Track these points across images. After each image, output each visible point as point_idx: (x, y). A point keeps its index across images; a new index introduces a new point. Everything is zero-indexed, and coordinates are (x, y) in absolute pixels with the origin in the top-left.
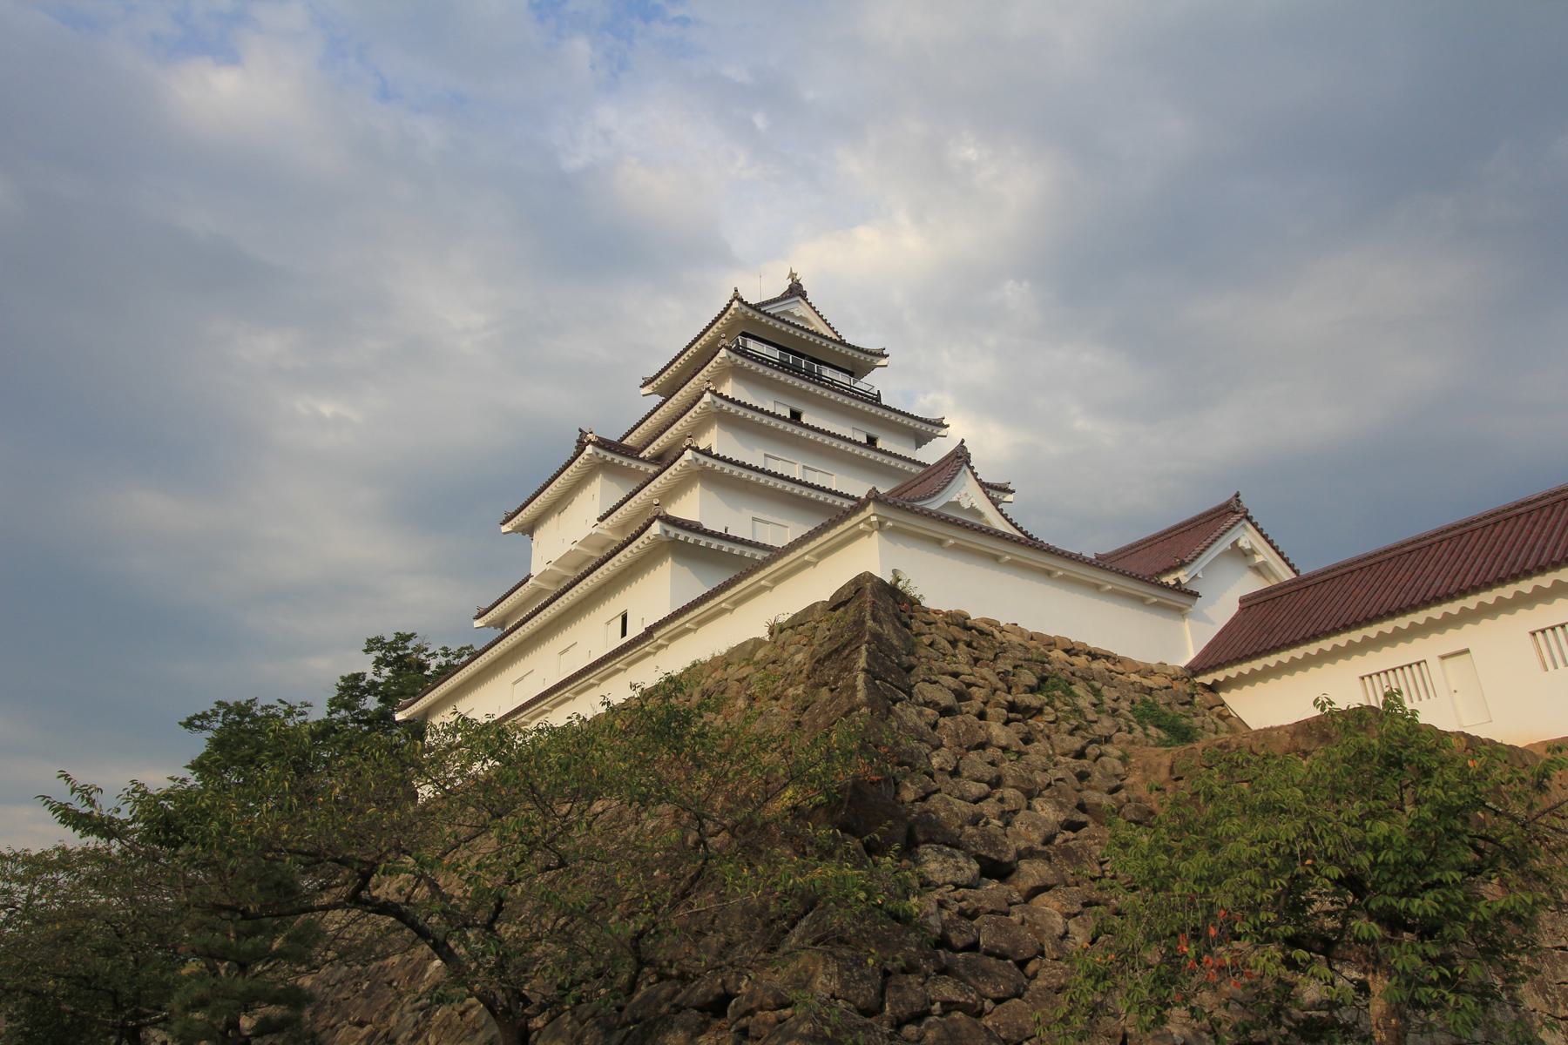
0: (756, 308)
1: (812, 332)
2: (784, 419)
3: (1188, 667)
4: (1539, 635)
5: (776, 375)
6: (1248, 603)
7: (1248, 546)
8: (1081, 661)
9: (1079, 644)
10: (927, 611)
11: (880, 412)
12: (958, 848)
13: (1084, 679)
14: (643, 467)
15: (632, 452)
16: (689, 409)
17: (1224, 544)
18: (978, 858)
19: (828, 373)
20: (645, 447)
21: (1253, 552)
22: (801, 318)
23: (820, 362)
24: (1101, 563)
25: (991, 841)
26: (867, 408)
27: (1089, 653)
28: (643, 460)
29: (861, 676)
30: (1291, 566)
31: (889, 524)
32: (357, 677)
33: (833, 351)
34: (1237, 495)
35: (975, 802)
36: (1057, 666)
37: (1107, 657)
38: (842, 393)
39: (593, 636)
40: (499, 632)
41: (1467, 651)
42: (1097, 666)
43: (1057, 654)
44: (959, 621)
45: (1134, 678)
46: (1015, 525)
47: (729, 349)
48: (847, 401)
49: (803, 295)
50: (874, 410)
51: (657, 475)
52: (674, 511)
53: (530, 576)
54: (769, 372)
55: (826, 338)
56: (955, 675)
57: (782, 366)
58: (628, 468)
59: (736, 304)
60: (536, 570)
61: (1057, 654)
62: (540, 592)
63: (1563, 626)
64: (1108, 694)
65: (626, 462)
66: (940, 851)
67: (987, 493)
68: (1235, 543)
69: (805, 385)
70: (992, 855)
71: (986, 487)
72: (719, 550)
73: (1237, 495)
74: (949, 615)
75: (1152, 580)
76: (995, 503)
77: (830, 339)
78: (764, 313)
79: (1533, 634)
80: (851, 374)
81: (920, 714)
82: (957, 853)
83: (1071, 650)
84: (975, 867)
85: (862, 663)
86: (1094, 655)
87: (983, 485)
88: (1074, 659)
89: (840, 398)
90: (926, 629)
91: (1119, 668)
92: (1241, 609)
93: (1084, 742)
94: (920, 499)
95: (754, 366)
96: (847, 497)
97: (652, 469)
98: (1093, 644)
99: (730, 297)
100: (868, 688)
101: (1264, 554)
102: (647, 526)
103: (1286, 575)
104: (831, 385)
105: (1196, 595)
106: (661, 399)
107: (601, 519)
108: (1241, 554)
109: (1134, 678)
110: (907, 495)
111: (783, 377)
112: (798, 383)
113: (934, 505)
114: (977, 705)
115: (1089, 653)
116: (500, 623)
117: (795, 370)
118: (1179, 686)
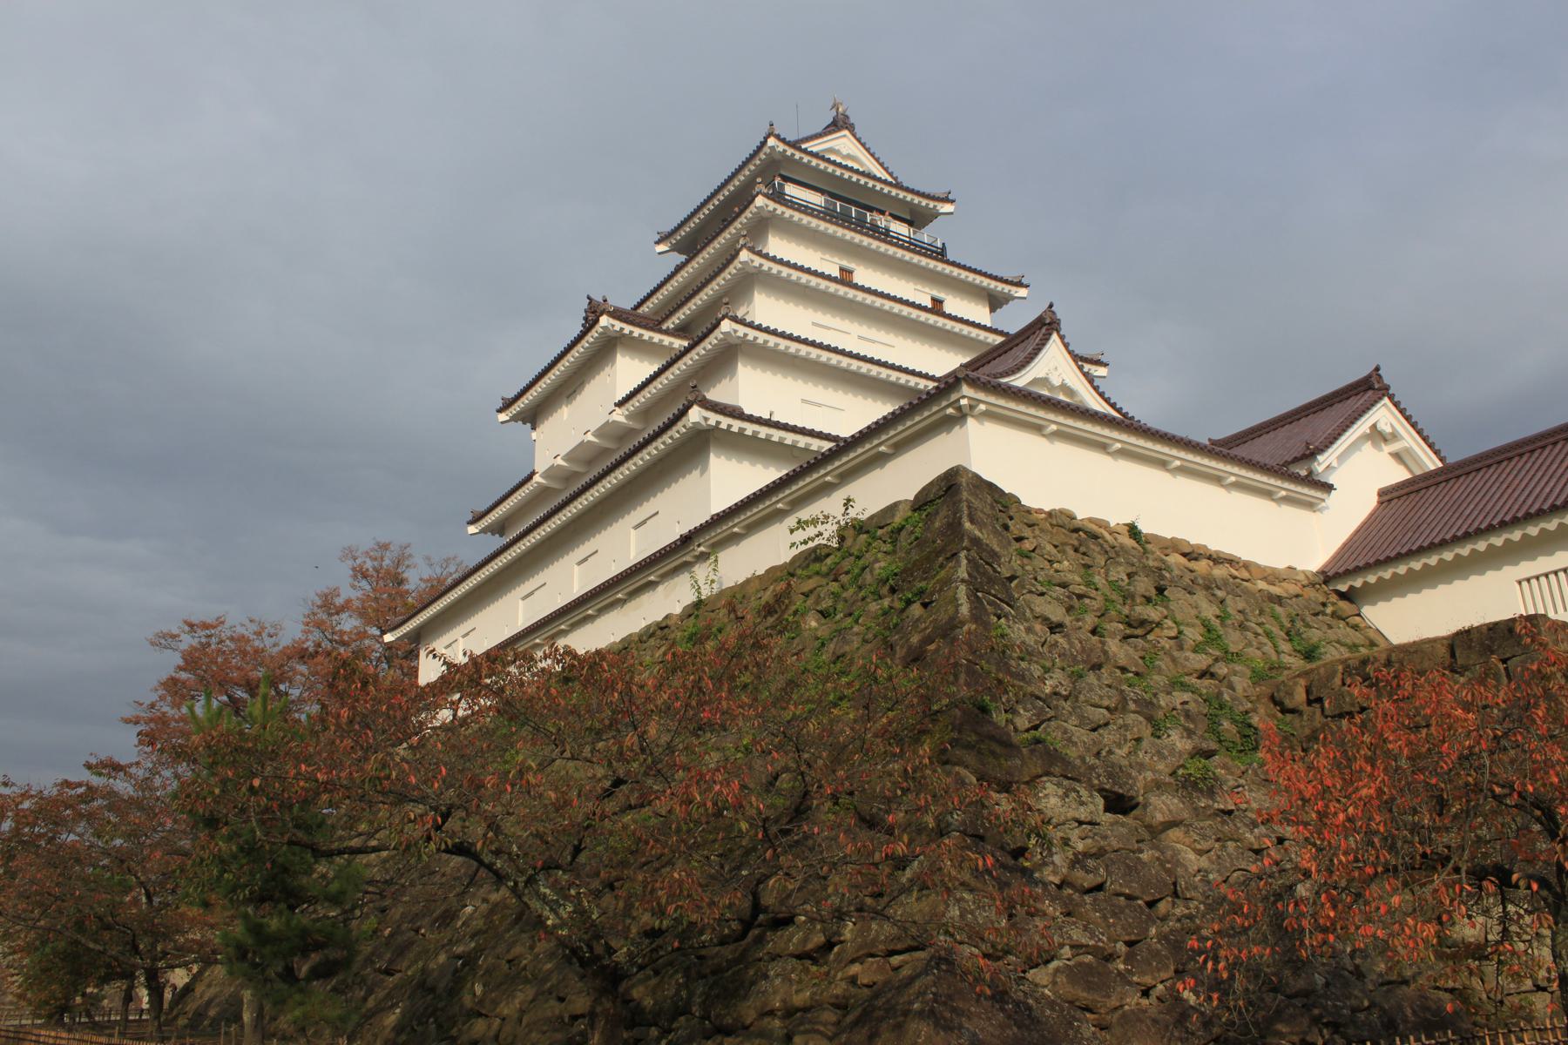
0: (795, 145)
1: (863, 174)
2: (925, 309)
3: (1322, 572)
4: (1525, 584)
5: (823, 226)
6: (1388, 496)
7: (1388, 430)
8: (1202, 566)
9: (1199, 546)
10: (1029, 511)
11: (948, 269)
12: (1079, 781)
13: (1207, 588)
14: (667, 340)
15: (654, 324)
16: (721, 270)
17: (1362, 427)
18: (1101, 791)
19: (882, 221)
20: (668, 317)
21: (1395, 436)
22: (849, 157)
23: (871, 209)
24: (1224, 449)
25: (1114, 772)
26: (932, 264)
27: (1210, 558)
28: (667, 332)
29: (963, 589)
30: (1436, 453)
31: (982, 407)
32: (335, 592)
33: (888, 195)
34: (1377, 369)
35: (1094, 730)
36: (1176, 572)
37: (1232, 561)
38: (902, 247)
39: (623, 543)
40: (498, 542)
41: (804, 401)
42: (1220, 572)
43: (1175, 559)
44: (1061, 521)
45: (1262, 585)
46: (1113, 406)
47: (766, 196)
48: (908, 256)
49: (851, 128)
50: (940, 266)
51: (687, 350)
52: (715, 394)
53: (533, 473)
54: (814, 222)
55: (879, 180)
56: (1064, 585)
57: (827, 215)
58: (640, 339)
59: (772, 142)
60: (541, 465)
61: (1175, 559)
62: (543, 493)
63: (1565, 570)
64: (1234, 605)
65: (647, 335)
66: (1059, 785)
67: (1081, 368)
68: (1374, 426)
69: (858, 238)
70: (1116, 789)
71: (1078, 359)
72: (755, 436)
73: (1377, 369)
74: (1050, 514)
75: (1281, 471)
76: (1090, 379)
77: (885, 182)
78: (805, 151)
79: (1520, 583)
80: (910, 223)
81: (1029, 630)
82: (1077, 786)
83: (1192, 554)
84: (1100, 802)
85: (963, 573)
86: (1217, 559)
87: (1076, 358)
88: (1193, 565)
89: (900, 253)
90: (1027, 532)
91: (1246, 575)
92: (1380, 503)
93: (1210, 661)
94: (1007, 374)
95: (797, 216)
96: (926, 377)
97: (679, 343)
98: (1214, 546)
99: (766, 129)
100: (971, 602)
101: (1409, 440)
102: (683, 413)
103: (1432, 463)
104: (897, 242)
105: (1329, 488)
106: (683, 258)
107: (620, 404)
108: (1377, 436)
109: (1262, 585)
110: (986, 369)
111: (831, 229)
112: (849, 235)
113: (1020, 380)
114: (1090, 620)
115: (1210, 558)
116: (500, 528)
117: (843, 220)
118: (1310, 593)
